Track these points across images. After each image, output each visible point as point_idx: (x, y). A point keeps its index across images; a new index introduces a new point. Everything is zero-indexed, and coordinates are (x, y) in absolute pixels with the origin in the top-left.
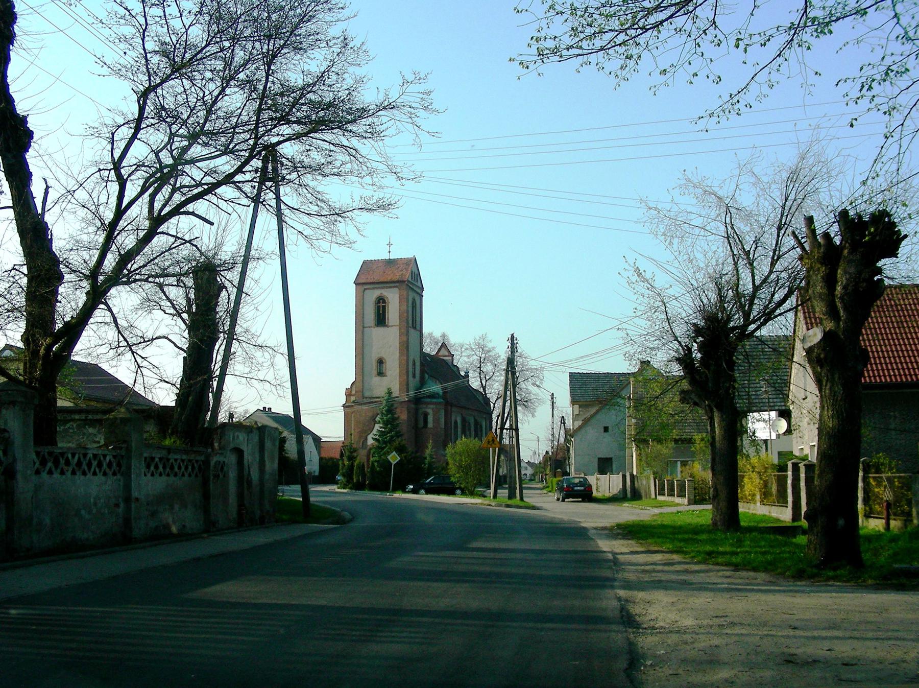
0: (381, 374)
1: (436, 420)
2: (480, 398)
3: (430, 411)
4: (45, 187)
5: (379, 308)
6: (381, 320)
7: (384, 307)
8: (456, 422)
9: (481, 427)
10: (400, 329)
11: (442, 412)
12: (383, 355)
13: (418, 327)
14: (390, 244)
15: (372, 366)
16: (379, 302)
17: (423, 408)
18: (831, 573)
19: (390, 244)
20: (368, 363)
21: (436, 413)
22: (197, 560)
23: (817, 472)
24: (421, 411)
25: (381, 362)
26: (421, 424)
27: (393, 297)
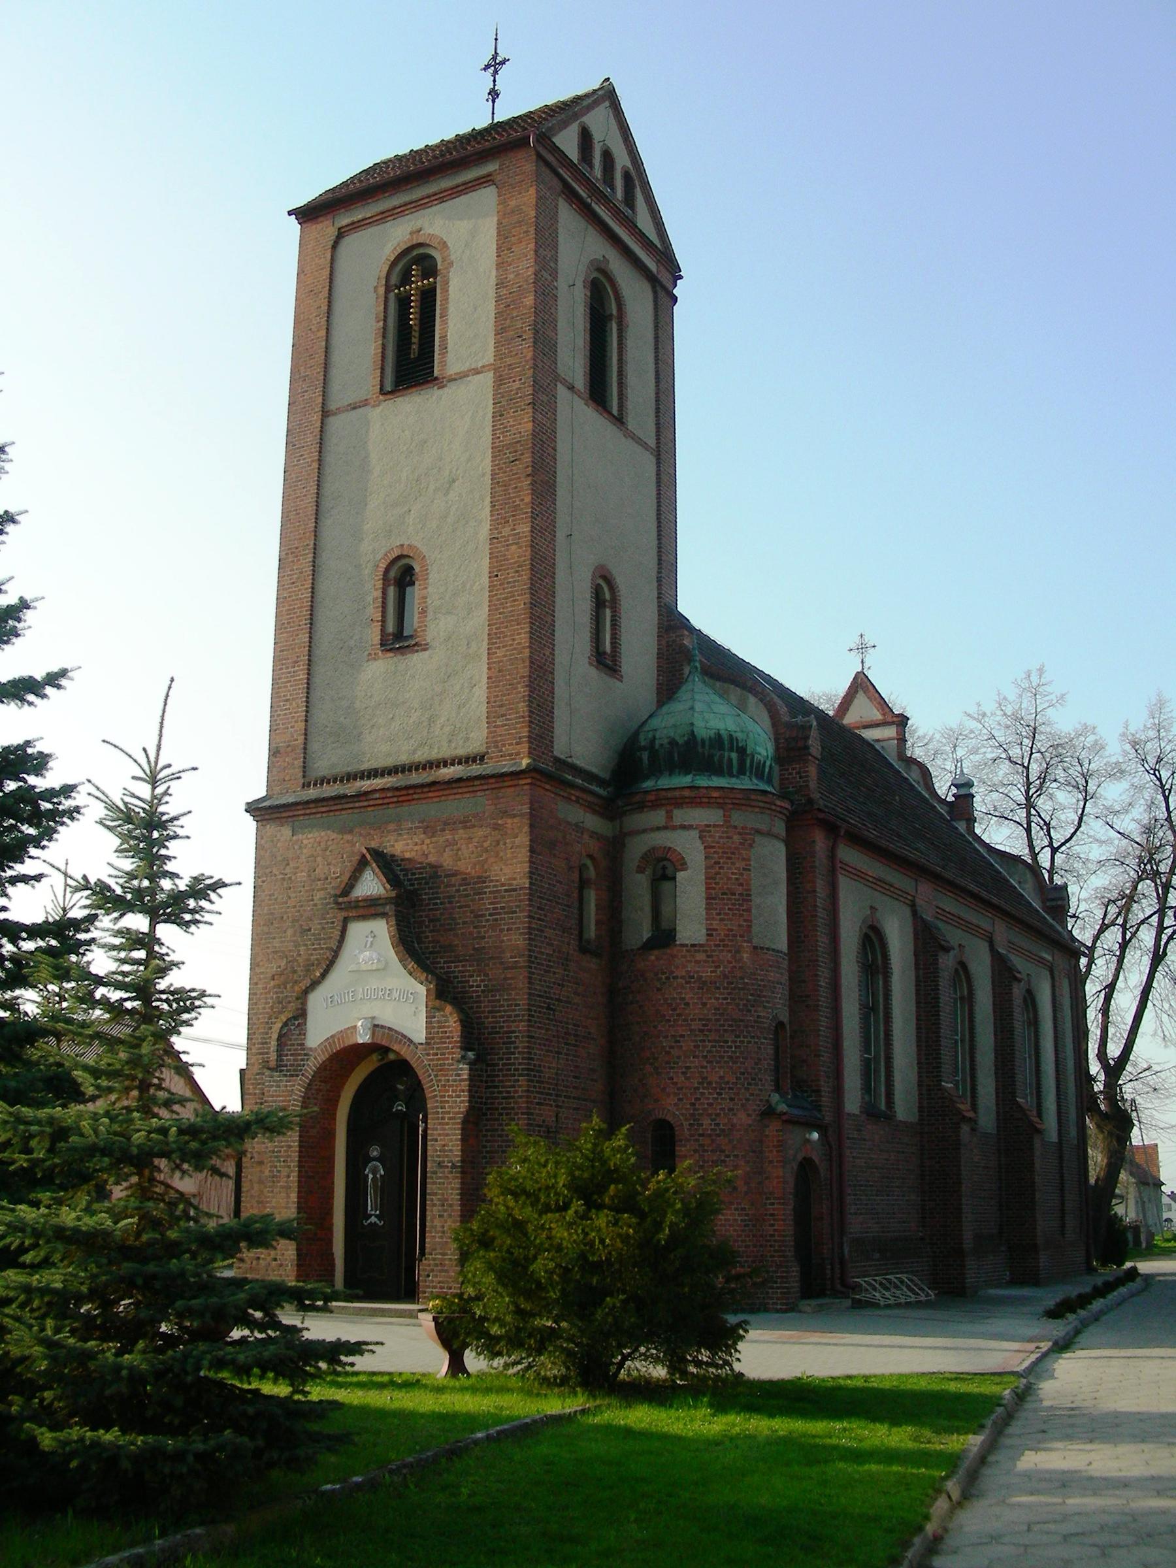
0: (398, 639)
1: (731, 899)
2: (1028, 892)
3: (689, 847)
4: (39, 676)
5: (403, 303)
6: (412, 361)
7: (429, 298)
8: (873, 940)
9: (1030, 999)
10: (499, 381)
11: (772, 857)
12: (413, 537)
13: (640, 417)
14: (495, 65)
15: (357, 598)
16: (405, 279)
17: (653, 831)
18: (945, 1423)
19: (495, 65)
20: (343, 597)
21: (724, 857)
22: (1032, 1494)
23: (140, 1550)
24: (637, 848)
25: (402, 576)
26: (640, 929)
27: (470, 238)
